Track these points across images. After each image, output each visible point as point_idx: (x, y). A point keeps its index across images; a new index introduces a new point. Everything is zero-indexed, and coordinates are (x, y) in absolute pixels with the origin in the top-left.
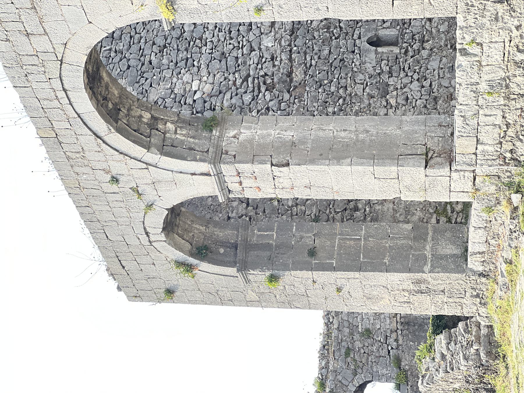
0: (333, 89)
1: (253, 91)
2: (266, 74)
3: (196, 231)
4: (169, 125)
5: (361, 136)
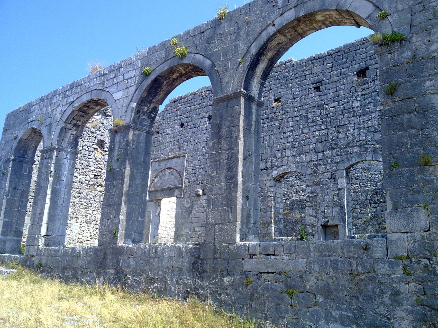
0: (92, 202)
1: (95, 171)
2: (101, 176)
3: (32, 142)
4: (75, 132)
5: (59, 209)
